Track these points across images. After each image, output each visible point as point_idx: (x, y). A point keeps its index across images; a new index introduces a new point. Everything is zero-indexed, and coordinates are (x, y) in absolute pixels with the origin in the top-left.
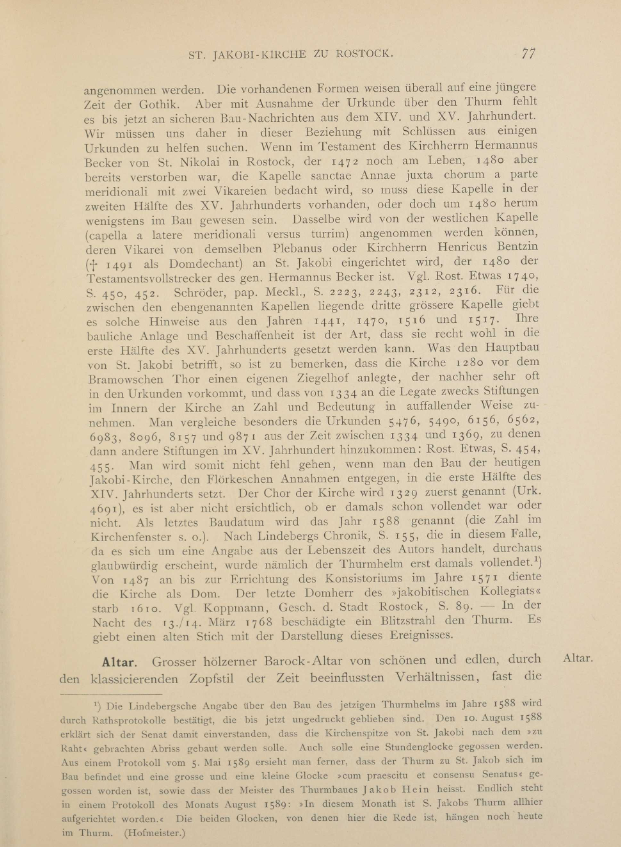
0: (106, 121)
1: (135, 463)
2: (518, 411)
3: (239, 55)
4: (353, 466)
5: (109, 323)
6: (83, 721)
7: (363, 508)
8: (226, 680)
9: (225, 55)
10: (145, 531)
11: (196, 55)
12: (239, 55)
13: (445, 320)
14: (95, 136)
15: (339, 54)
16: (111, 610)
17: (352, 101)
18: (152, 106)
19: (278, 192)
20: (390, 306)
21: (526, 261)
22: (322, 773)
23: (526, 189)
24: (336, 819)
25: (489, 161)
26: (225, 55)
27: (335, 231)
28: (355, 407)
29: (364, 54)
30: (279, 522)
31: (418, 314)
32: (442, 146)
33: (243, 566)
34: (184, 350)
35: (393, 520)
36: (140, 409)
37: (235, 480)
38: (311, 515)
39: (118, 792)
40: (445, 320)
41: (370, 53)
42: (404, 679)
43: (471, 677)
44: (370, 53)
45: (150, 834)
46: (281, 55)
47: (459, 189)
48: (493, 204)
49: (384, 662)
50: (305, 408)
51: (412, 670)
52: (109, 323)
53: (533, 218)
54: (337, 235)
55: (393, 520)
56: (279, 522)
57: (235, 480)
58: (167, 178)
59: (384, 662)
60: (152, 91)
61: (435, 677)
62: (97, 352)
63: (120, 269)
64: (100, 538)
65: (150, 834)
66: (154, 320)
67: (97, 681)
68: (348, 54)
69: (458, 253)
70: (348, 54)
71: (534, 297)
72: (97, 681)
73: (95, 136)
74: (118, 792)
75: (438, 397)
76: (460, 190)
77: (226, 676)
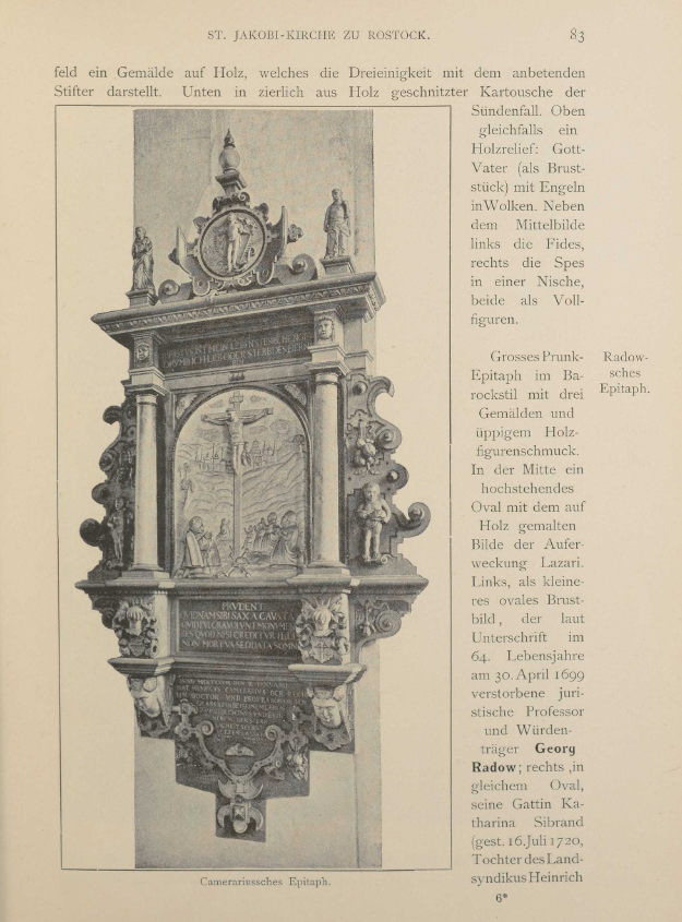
0: (475, 620)
1: (529, 466)
3: (262, 35)
8: (509, 396)
11: (216, 35)
12: (262, 35)
15: (371, 35)
17: (188, 89)
18: (567, 150)
19: (475, 302)
20: (576, 150)
21: (571, 93)
36: (537, 527)
38: (523, 254)
39: (555, 526)
41: (404, 35)
42: (562, 303)
45: (248, 883)
46: (308, 36)
47: (490, 91)
50: (579, 823)
62: (490, 695)
65: (248, 883)
67: (550, 583)
72: (550, 583)
74: (555, 526)
76: (572, 805)
77: (509, 391)
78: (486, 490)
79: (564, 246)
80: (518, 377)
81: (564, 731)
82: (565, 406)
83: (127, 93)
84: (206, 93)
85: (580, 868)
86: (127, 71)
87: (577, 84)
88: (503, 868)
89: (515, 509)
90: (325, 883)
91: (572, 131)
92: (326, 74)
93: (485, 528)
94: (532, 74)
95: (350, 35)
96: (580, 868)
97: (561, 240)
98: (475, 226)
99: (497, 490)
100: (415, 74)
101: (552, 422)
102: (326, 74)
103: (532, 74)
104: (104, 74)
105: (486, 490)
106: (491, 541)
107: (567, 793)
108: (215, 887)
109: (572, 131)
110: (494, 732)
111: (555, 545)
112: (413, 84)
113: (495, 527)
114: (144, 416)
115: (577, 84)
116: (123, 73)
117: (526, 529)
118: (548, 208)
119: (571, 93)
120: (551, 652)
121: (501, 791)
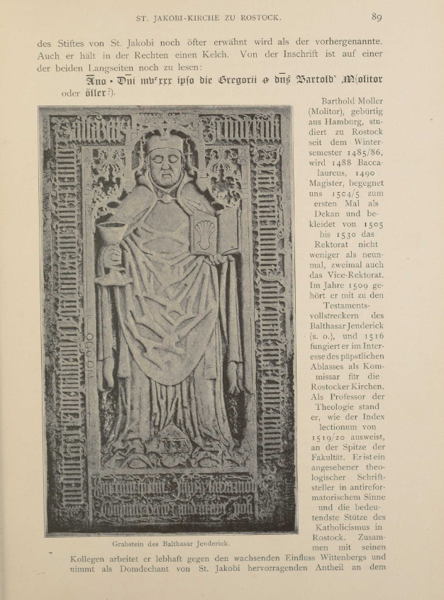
2: (369, 401)
3: (172, 18)
4: (341, 266)
6: (177, 43)
7: (347, 428)
9: (162, 18)
10: (351, 261)
11: (142, 19)
12: (172, 18)
13: (378, 557)
14: (362, 143)
23: (376, 397)
25: (356, 153)
26: (162, 18)
29: (261, 17)
30: (330, 418)
31: (357, 117)
32: (373, 356)
34: (364, 213)
35: (346, 162)
36: (354, 316)
37: (341, 387)
40: (378, 557)
41: (265, 18)
42: (246, 56)
44: (265, 18)
49: (112, 560)
50: (383, 557)
51: (129, 565)
53: (381, 477)
55: (346, 162)
56: (330, 418)
57: (341, 387)
58: (328, 42)
59: (112, 560)
61: (143, 569)
63: (365, 176)
68: (249, 18)
69: (376, 441)
70: (249, 18)
71: (381, 452)
73: (362, 143)
75: (364, 270)
78: (323, 428)
81: (372, 174)
82: (374, 403)
85: (382, 472)
87: (380, 442)
88: (324, 321)
91: (377, 377)
94: (349, 558)
95: (230, 18)
96: (382, 472)
97: (69, 66)
98: (39, 69)
99: (374, 132)
101: (362, 240)
103: (349, 558)
105: (323, 428)
106: (69, 66)
107: (373, 147)
108: (159, 23)
109: (377, 377)
110: (325, 508)
111: (44, 57)
113: (322, 112)
114: (105, 330)
115: (380, 442)
119: (325, 337)
120: (360, 323)
121: (193, 71)
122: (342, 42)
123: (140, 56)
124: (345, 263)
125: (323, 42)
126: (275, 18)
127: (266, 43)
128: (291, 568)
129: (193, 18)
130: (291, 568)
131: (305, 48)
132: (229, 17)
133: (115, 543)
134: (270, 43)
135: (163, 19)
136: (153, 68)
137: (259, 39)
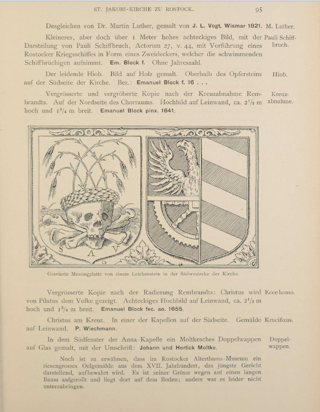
3: (118, 9)
5: (63, 380)
11: (97, 9)
12: (118, 9)
16: (177, 366)
22: (206, 273)
24: (159, 274)
27: (130, 53)
28: (51, 301)
29: (179, 9)
33: (257, 293)
36: (162, 293)
41: (182, 9)
42: (80, 302)
43: (176, 380)
44: (182, 9)
48: (180, 309)
50: (52, 310)
52: (63, 380)
54: (231, 373)
60: (44, 111)
64: (269, 321)
66: (163, 101)
68: (171, 9)
70: (171, 9)
76: (145, 340)
79: (68, 75)
80: (100, 74)
83: (35, 46)
84: (69, 83)
86: (177, 372)
89: (242, 38)
90: (285, 45)
92: (72, 111)
93: (90, 75)
94: (85, 38)
100: (47, 55)
102: (72, 111)
104: (173, 340)
108: (110, 12)
111: (58, 103)
112: (205, 297)
113: (187, 340)
116: (183, 339)
117: (160, 75)
118: (81, 103)
122: (56, 94)
123: (251, 94)
124: (154, 53)
125: (89, 27)
126: (189, 9)
127: (257, 293)
128: (250, 55)
129: (133, 9)
130: (250, 55)
131: (83, 344)
132: (158, 9)
133: (175, 372)
134: (259, 293)
135: (112, 10)
136: (36, 310)
137: (252, 291)
